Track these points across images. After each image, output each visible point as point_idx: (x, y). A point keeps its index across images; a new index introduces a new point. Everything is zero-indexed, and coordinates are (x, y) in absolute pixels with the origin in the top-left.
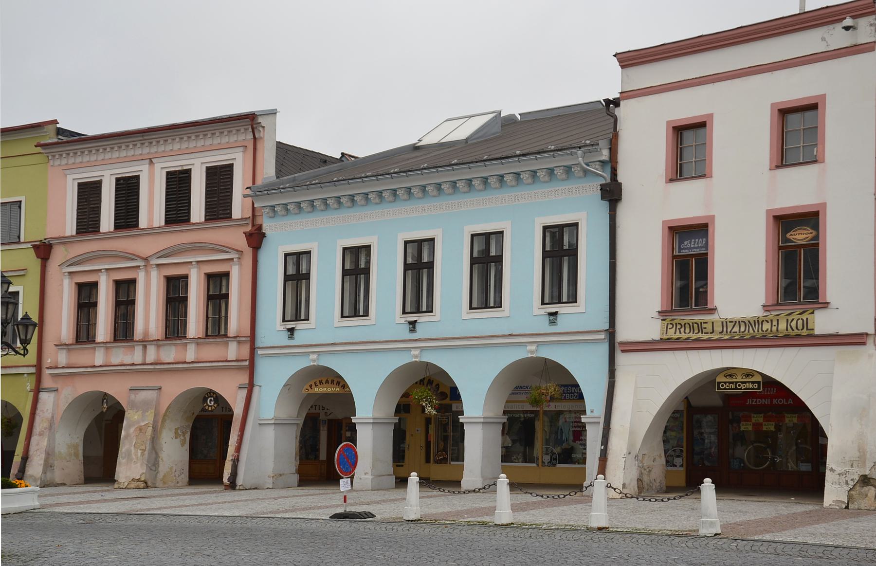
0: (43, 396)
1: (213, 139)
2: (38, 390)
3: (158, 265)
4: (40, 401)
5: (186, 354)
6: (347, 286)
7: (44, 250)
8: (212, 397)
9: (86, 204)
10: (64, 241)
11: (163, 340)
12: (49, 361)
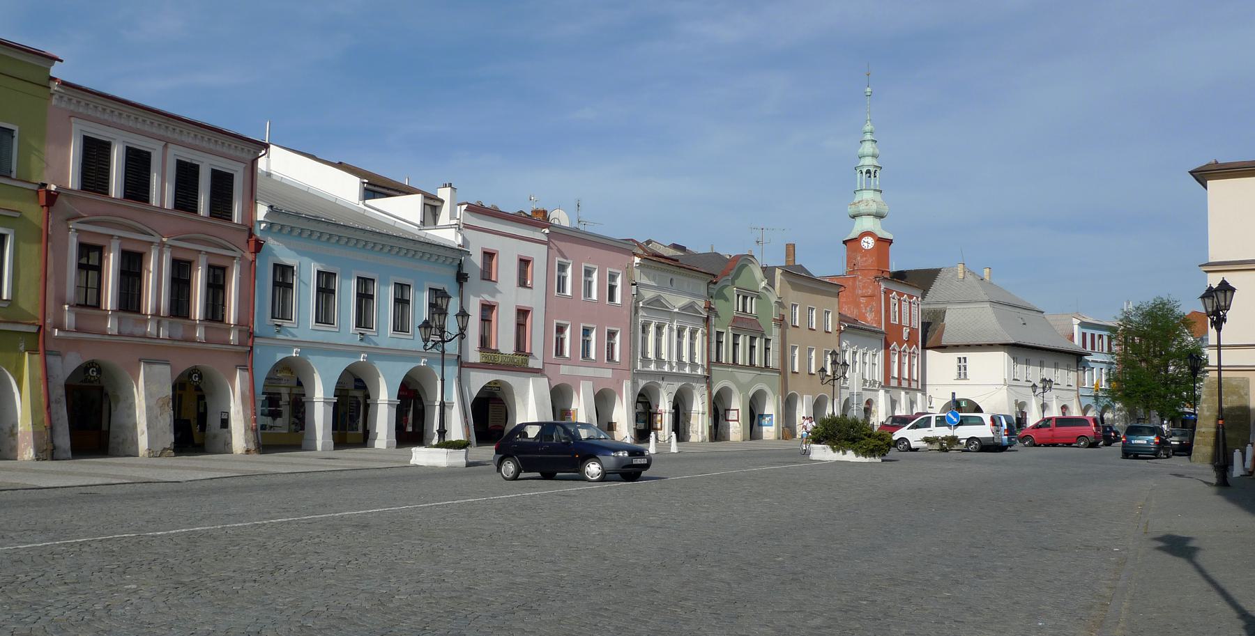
5: (76, 324)
6: (210, 294)
8: (94, 367)
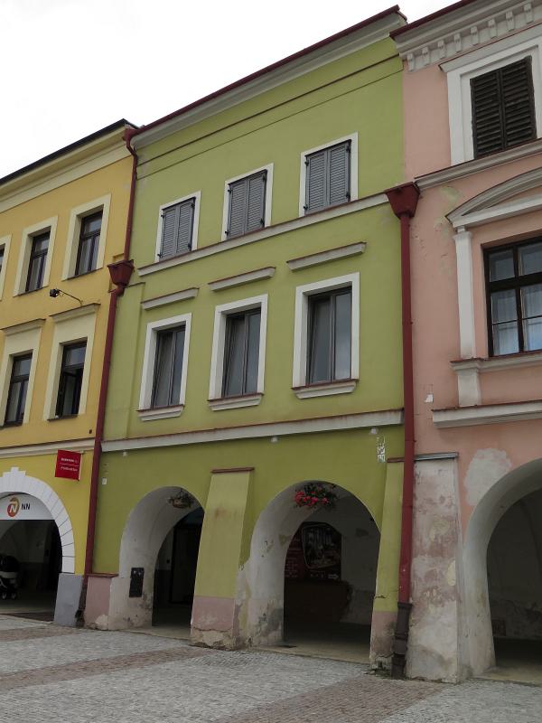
0: (425, 470)
1: (515, 21)
2: (410, 459)
3: (468, 228)
4: (418, 480)
7: (405, 201)
9: (495, 104)
10: (449, 176)
11: (148, 410)
12: (430, 399)
